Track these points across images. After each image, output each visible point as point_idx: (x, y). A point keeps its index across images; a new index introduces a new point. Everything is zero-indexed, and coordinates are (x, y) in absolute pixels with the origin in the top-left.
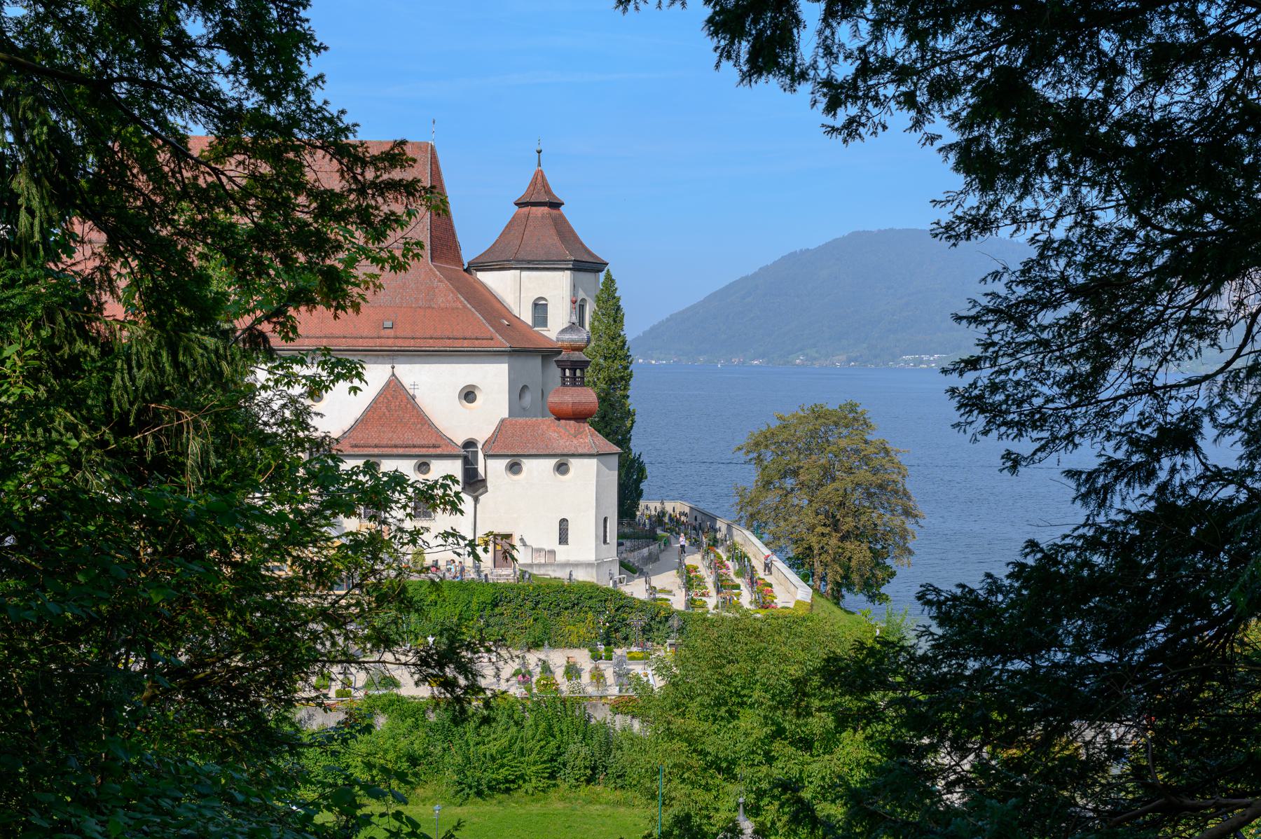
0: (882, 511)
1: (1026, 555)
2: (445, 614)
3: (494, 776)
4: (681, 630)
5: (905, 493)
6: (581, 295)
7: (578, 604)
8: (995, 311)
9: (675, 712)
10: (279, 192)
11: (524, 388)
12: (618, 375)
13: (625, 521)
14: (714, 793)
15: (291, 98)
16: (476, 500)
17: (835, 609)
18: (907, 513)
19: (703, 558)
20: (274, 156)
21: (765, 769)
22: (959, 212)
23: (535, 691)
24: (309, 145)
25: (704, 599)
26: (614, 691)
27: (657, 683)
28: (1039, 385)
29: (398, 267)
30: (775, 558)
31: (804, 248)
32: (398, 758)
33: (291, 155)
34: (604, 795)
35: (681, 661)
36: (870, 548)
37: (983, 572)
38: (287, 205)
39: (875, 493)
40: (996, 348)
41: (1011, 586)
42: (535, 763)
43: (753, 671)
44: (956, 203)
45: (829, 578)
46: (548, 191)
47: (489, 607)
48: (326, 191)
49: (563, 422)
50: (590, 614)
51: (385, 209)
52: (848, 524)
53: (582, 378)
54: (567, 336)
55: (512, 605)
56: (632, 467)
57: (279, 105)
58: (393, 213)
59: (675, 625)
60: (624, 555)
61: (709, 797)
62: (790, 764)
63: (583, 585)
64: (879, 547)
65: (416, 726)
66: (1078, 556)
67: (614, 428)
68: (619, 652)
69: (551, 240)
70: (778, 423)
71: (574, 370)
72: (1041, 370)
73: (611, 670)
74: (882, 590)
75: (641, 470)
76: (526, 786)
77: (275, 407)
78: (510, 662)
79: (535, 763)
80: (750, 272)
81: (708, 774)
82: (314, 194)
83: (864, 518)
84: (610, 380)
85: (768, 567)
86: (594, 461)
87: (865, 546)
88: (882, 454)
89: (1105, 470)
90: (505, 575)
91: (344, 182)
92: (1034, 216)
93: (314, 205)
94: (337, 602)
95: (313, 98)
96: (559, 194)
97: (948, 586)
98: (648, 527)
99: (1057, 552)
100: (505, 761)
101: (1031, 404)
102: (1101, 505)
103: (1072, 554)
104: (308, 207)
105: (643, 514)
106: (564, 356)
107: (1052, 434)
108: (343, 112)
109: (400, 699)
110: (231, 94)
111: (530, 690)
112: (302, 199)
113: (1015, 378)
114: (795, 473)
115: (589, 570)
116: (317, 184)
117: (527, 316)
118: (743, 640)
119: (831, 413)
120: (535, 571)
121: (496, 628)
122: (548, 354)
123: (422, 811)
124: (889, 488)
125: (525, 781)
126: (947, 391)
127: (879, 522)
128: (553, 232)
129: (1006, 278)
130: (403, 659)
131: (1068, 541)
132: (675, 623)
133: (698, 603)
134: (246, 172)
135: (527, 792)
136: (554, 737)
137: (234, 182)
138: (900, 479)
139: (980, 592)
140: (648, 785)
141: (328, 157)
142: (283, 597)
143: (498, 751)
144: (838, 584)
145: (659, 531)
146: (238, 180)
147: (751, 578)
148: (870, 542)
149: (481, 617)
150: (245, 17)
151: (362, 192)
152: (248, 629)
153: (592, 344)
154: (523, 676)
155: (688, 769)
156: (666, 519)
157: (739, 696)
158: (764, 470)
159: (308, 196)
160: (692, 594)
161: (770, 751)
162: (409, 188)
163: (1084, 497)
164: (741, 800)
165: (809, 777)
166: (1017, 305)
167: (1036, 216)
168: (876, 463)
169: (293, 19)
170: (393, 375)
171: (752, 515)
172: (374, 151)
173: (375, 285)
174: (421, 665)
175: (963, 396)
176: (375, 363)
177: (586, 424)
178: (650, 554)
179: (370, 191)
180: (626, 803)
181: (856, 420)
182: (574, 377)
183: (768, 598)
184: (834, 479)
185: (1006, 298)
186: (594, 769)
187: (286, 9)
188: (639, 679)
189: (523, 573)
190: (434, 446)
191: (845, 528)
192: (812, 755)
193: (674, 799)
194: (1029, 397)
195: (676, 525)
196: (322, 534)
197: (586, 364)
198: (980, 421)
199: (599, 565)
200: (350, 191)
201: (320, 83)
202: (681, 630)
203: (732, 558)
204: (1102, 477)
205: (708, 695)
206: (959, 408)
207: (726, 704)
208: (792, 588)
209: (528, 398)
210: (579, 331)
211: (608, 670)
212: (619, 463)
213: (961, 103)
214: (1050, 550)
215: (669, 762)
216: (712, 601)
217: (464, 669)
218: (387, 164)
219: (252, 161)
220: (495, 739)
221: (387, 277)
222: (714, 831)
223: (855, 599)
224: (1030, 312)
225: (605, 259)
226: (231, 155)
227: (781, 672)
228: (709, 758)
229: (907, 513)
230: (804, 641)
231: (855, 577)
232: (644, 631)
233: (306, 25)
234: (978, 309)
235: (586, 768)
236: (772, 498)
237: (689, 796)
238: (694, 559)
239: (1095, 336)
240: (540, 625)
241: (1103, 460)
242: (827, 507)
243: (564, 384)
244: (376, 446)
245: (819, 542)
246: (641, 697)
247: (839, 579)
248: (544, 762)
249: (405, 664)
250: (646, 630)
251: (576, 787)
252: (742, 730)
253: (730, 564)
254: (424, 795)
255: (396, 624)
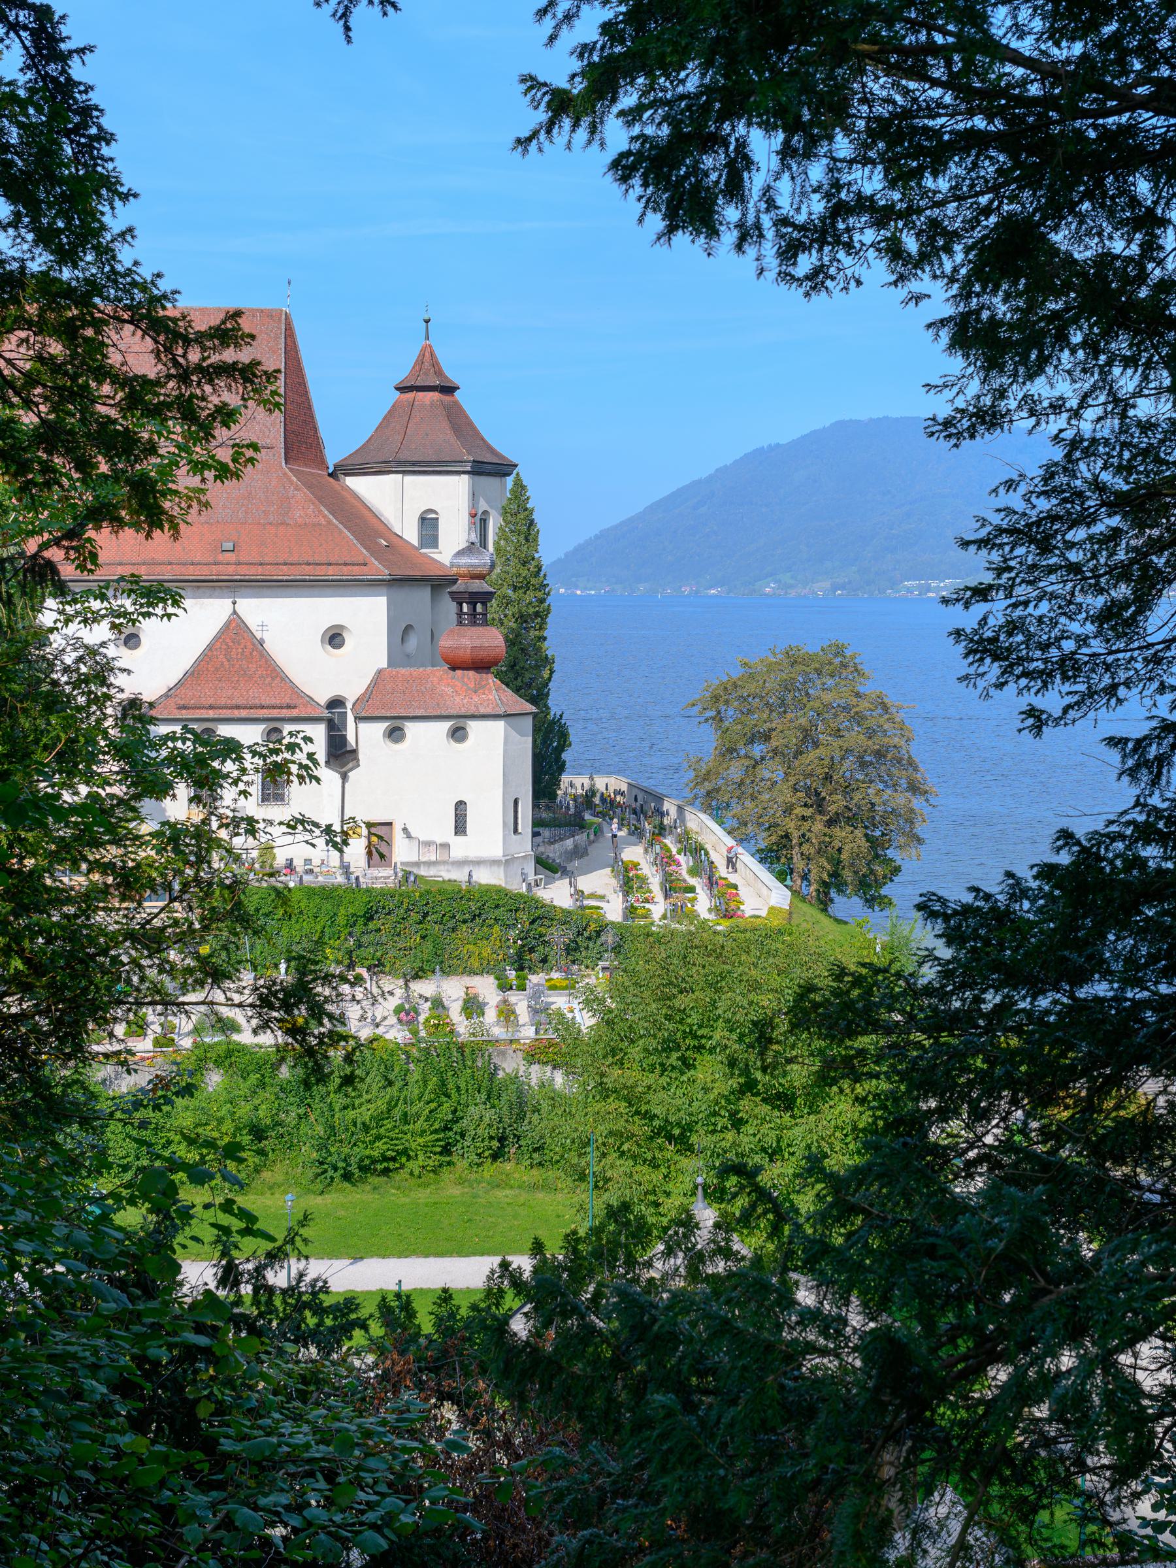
0: (881, 786)
1: (1059, 849)
2: (292, 935)
3: (367, 1152)
4: (617, 949)
5: (911, 763)
6: (483, 506)
7: (480, 915)
8: (1011, 531)
9: (610, 1059)
10: (74, 378)
11: (408, 628)
12: (531, 611)
13: (543, 803)
14: (664, 1170)
15: (89, 258)
16: (344, 777)
17: (821, 917)
18: (914, 788)
19: (646, 851)
20: (68, 332)
21: (730, 1135)
22: (960, 403)
23: (423, 1034)
24: (114, 318)
25: (647, 906)
26: (528, 1032)
27: (586, 1021)
28: (1067, 622)
29: (224, 472)
30: (740, 850)
31: (773, 442)
32: (238, 1129)
33: (89, 332)
34: (516, 1175)
35: (618, 991)
36: (866, 835)
37: (1002, 871)
38: (84, 396)
39: (871, 763)
40: (1013, 574)
41: (1040, 889)
42: (422, 1133)
43: (713, 1003)
44: (955, 389)
45: (812, 877)
46: (439, 372)
47: (361, 921)
48: (136, 377)
49: (459, 672)
50: (496, 928)
51: (215, 400)
52: (835, 804)
53: (485, 615)
54: (464, 560)
55: (393, 918)
56: (551, 731)
57: (75, 266)
58: (225, 404)
59: (610, 942)
60: (541, 849)
61: (657, 1177)
62: (765, 1129)
63: (487, 890)
64: (878, 833)
65: (262, 1085)
66: (1128, 848)
67: (526, 680)
68: (535, 979)
69: (444, 440)
70: (741, 671)
71: (473, 605)
72: (1070, 602)
73: (524, 1004)
74: (884, 891)
75: (563, 735)
76: (411, 1165)
77: (69, 660)
78: (381, 1000)
79: (422, 1133)
80: (704, 475)
81: (654, 1145)
82: (121, 380)
83: (857, 796)
84: (522, 616)
85: (731, 862)
86: (500, 725)
87: (859, 833)
88: (879, 711)
89: (1158, 737)
90: (381, 878)
91: (160, 366)
92: (1057, 407)
93: (120, 395)
94: (149, 922)
95: (120, 257)
96: (453, 375)
97: (958, 895)
98: (572, 811)
99: (1099, 844)
100: (382, 1131)
101: (1059, 648)
102: (1155, 782)
103: (1120, 846)
104: (113, 398)
105: (565, 794)
106: (460, 586)
107: (1089, 688)
108: (159, 275)
109: (243, 1049)
110: (12, 253)
111: (415, 1033)
112: (106, 389)
113: (1037, 613)
114: (766, 737)
115: (495, 868)
116: (125, 368)
117: (411, 534)
118: (699, 961)
119: (812, 658)
120: (423, 872)
121: (371, 950)
122: (439, 583)
123: (268, 1202)
124: (889, 756)
125: (409, 1158)
126: (950, 634)
127: (876, 800)
128: (445, 424)
129: (1023, 489)
130: (237, 998)
131: (1114, 828)
132: (609, 938)
133: (639, 912)
134: (31, 352)
135: (411, 1174)
136: (448, 1096)
137: (14, 366)
138: (903, 743)
139: (999, 897)
140: (575, 1161)
141: (139, 333)
142: (76, 916)
143: (372, 1118)
144: (825, 884)
145: (587, 816)
146: (20, 363)
147: (710, 878)
148: (866, 828)
149: (350, 934)
150: (30, 155)
151: (184, 377)
152: (27, 961)
153: (498, 570)
154: (407, 1014)
155: (628, 1139)
156: (597, 800)
157: (695, 1036)
158: (724, 733)
159: (113, 383)
160: (632, 899)
161: (737, 1112)
162: (246, 373)
163: (1133, 773)
164: (700, 1180)
165: (789, 1145)
166: (1038, 523)
167: (1060, 407)
168: (872, 723)
169: (93, 158)
170: (235, 612)
171: (708, 794)
172: (201, 325)
173: (199, 502)
174: (261, 1007)
175: (972, 640)
176: (210, 597)
177: (490, 676)
178: (576, 846)
179: (194, 378)
180: (545, 1186)
181: (844, 666)
182: (473, 614)
183: (732, 904)
184: (816, 744)
185: (1024, 514)
186: (502, 1139)
187: (84, 145)
188: (562, 1016)
189: (407, 874)
190: (289, 707)
191: (832, 809)
192: (793, 1117)
193: (610, 1180)
194: (1058, 639)
195: (609, 807)
196: (130, 831)
197: (490, 595)
198: (993, 670)
199: (508, 862)
200: (169, 377)
201: (129, 238)
202: (617, 949)
203: (684, 850)
204: (1154, 746)
205: (654, 1036)
206: (967, 655)
207: (678, 1047)
208: (765, 891)
209: (413, 642)
210: (480, 553)
211: (521, 1004)
212: (534, 726)
213: (957, 258)
214: (1090, 840)
215: (603, 1129)
216: (658, 909)
217: (318, 1011)
218: (216, 342)
219: (39, 338)
220: (369, 1101)
221: (218, 492)
222: (665, 1224)
223: (847, 904)
224: (1056, 532)
225: (515, 460)
226: (10, 331)
227: (751, 1003)
228: (656, 1123)
229: (914, 788)
230: (780, 961)
231: (848, 875)
232: (569, 950)
233: (110, 166)
234: (989, 528)
235: (491, 1138)
236: (735, 771)
237: (631, 1176)
238: (634, 853)
239: (1141, 555)
240: (429, 945)
241: (1154, 723)
242: (808, 782)
243: (460, 623)
244: (211, 707)
245: (798, 828)
246: (564, 1040)
247: (826, 877)
248: (436, 1132)
249: (240, 1005)
250: (571, 949)
251: (479, 1165)
252: (699, 1084)
253: (681, 858)
254: (272, 1181)
255: (227, 950)
